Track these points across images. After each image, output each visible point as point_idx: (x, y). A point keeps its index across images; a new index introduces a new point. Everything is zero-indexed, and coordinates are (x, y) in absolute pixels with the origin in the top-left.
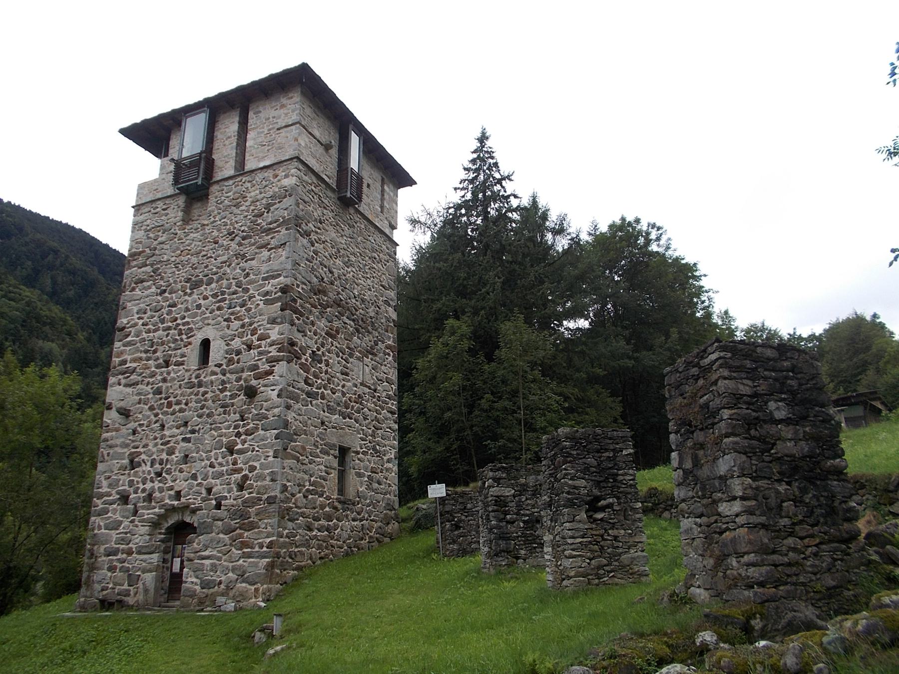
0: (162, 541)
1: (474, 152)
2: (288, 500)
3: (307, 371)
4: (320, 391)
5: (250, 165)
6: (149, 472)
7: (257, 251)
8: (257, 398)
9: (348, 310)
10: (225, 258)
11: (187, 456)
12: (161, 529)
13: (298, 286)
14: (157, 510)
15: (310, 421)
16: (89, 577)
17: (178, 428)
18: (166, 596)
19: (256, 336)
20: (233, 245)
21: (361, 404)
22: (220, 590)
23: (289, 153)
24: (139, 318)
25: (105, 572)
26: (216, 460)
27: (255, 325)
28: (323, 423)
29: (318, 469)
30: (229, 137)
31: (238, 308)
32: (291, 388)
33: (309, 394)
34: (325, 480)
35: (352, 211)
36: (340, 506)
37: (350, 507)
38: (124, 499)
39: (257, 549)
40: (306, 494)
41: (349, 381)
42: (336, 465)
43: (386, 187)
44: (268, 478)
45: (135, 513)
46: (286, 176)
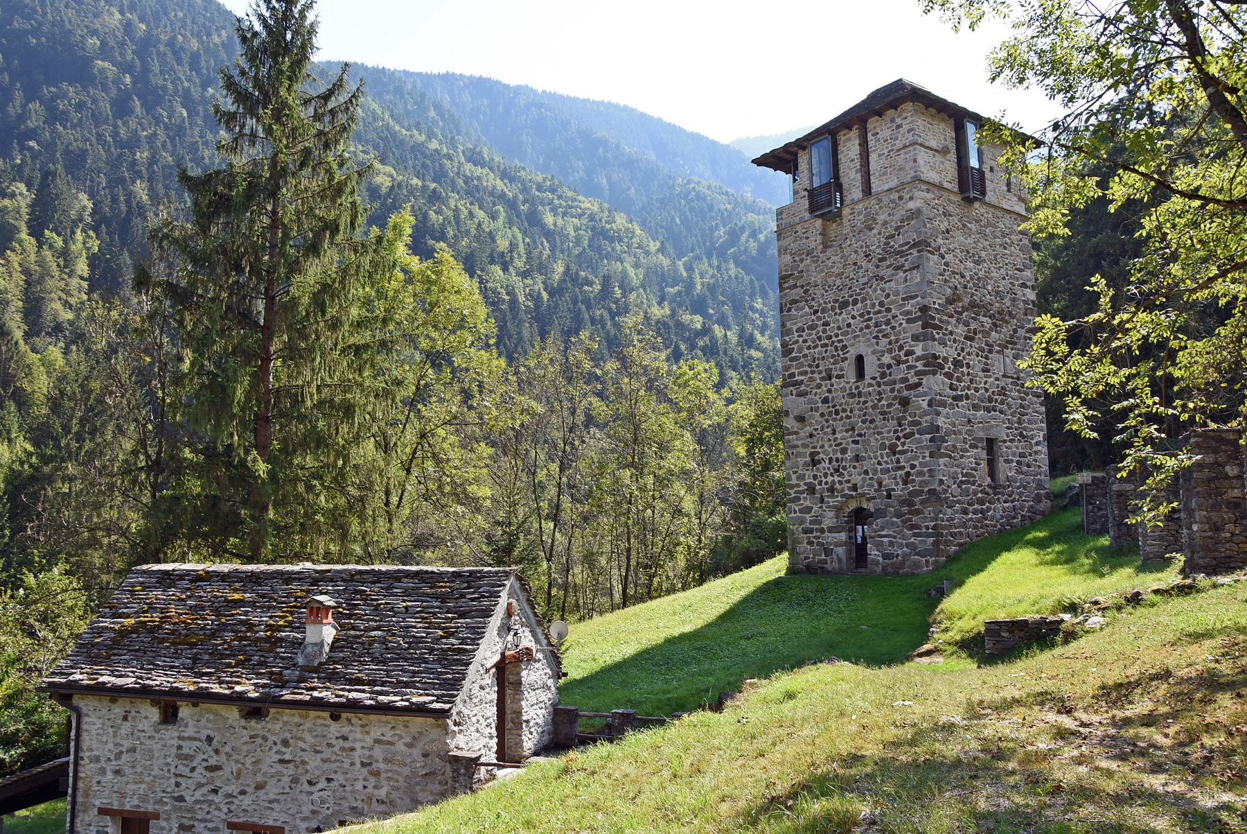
0: (846, 522)
5: (876, 185)
10: (865, 280)
28: (969, 421)
29: (969, 461)
33: (955, 398)
38: (811, 490)
42: (985, 456)
45: (822, 501)
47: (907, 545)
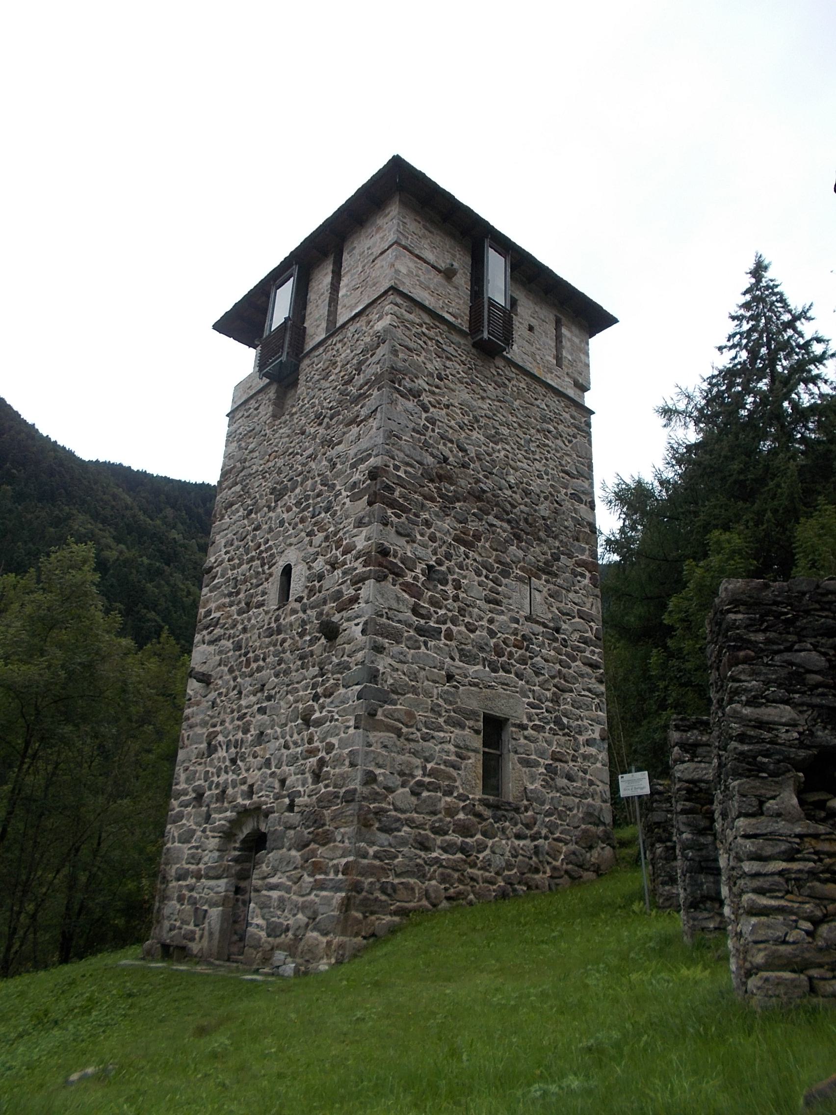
0: (236, 860)
1: (744, 294)
3: (418, 595)
4: (444, 627)
7: (345, 430)
8: (339, 640)
9: (497, 505)
12: (235, 842)
13: (397, 468)
14: (228, 814)
15: (423, 673)
16: (159, 908)
17: (255, 695)
22: (287, 940)
23: (386, 285)
25: (173, 905)
26: (291, 737)
27: (341, 534)
28: (450, 677)
30: (322, 294)
31: (323, 515)
32: (384, 620)
33: (420, 631)
35: (500, 363)
36: (487, 813)
39: (332, 876)
40: (418, 790)
43: (564, 331)
44: (347, 763)
47: (303, 908)
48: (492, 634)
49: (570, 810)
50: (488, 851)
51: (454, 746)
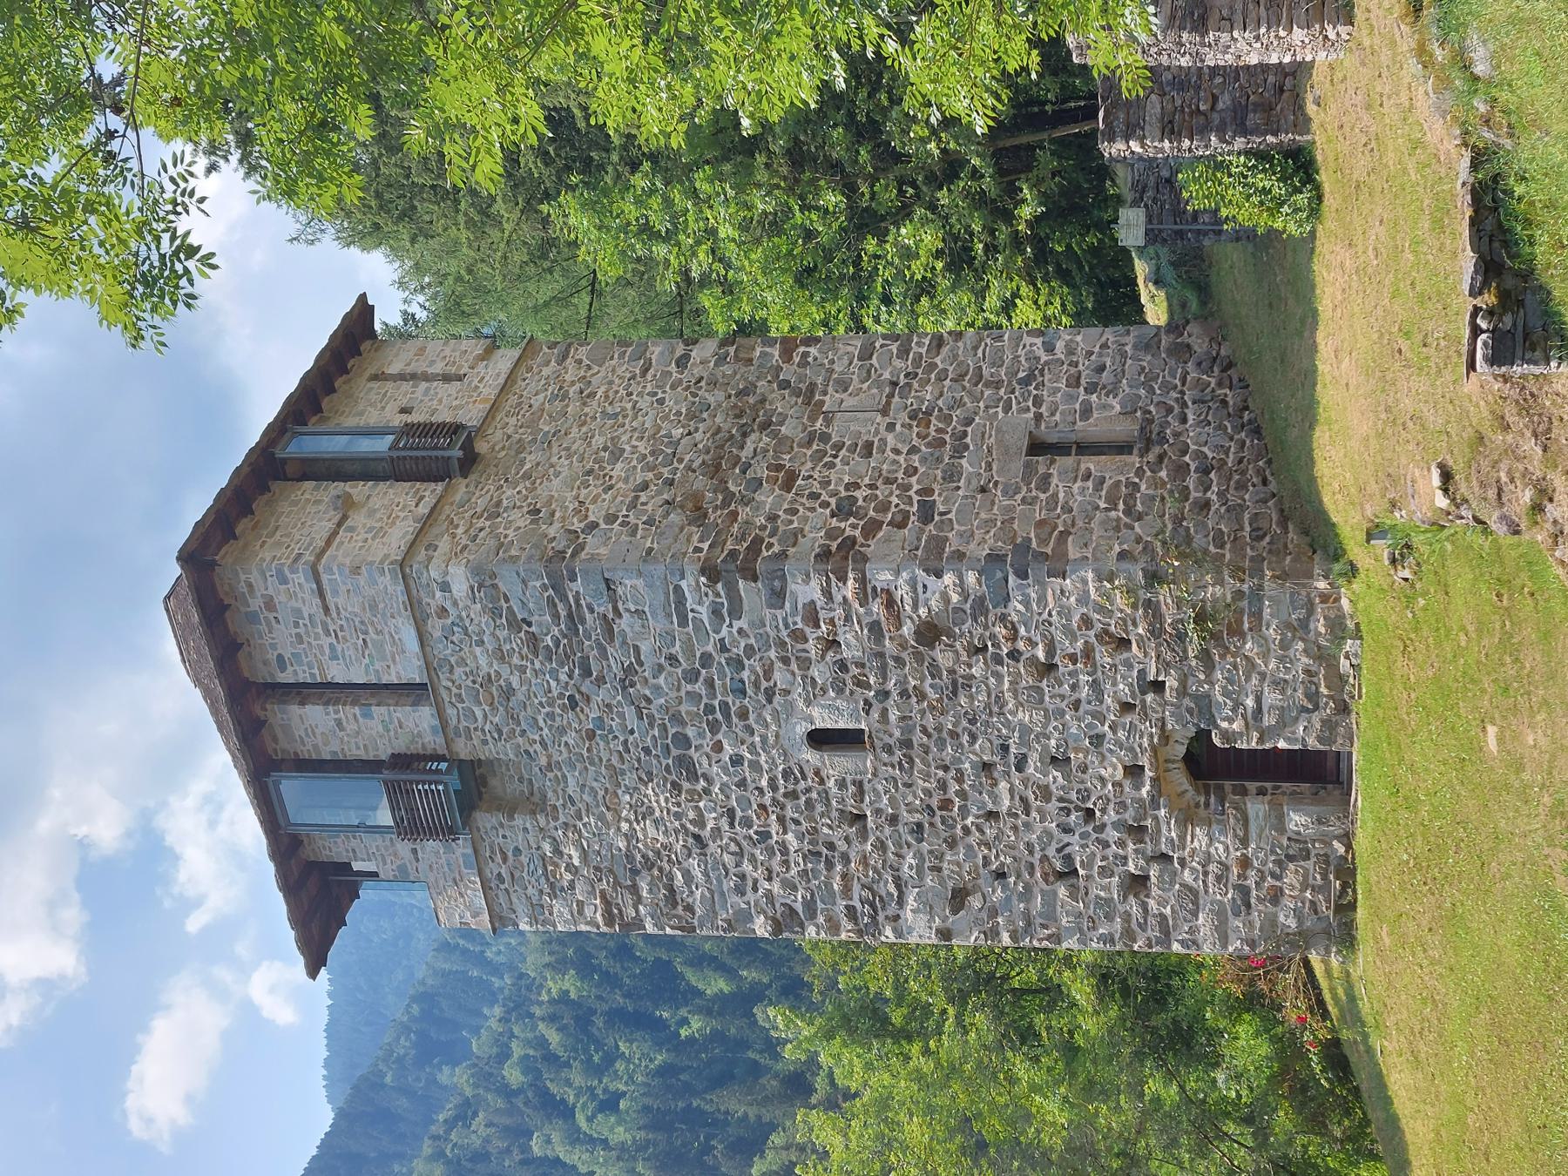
2: (1148, 548)
3: (878, 525)
4: (916, 498)
5: (409, 669)
6: (1084, 836)
10: (630, 712)
11: (1054, 759)
13: (698, 550)
18: (1330, 786)
19: (808, 630)
20: (601, 696)
21: (928, 413)
24: (755, 889)
28: (983, 490)
30: (339, 723)
34: (1102, 481)
36: (1157, 450)
37: (1155, 428)
41: (883, 441)
43: (393, 369)
46: (445, 587)
48: (913, 450)
49: (1143, 368)
50: (1205, 449)
51: (1070, 485)
